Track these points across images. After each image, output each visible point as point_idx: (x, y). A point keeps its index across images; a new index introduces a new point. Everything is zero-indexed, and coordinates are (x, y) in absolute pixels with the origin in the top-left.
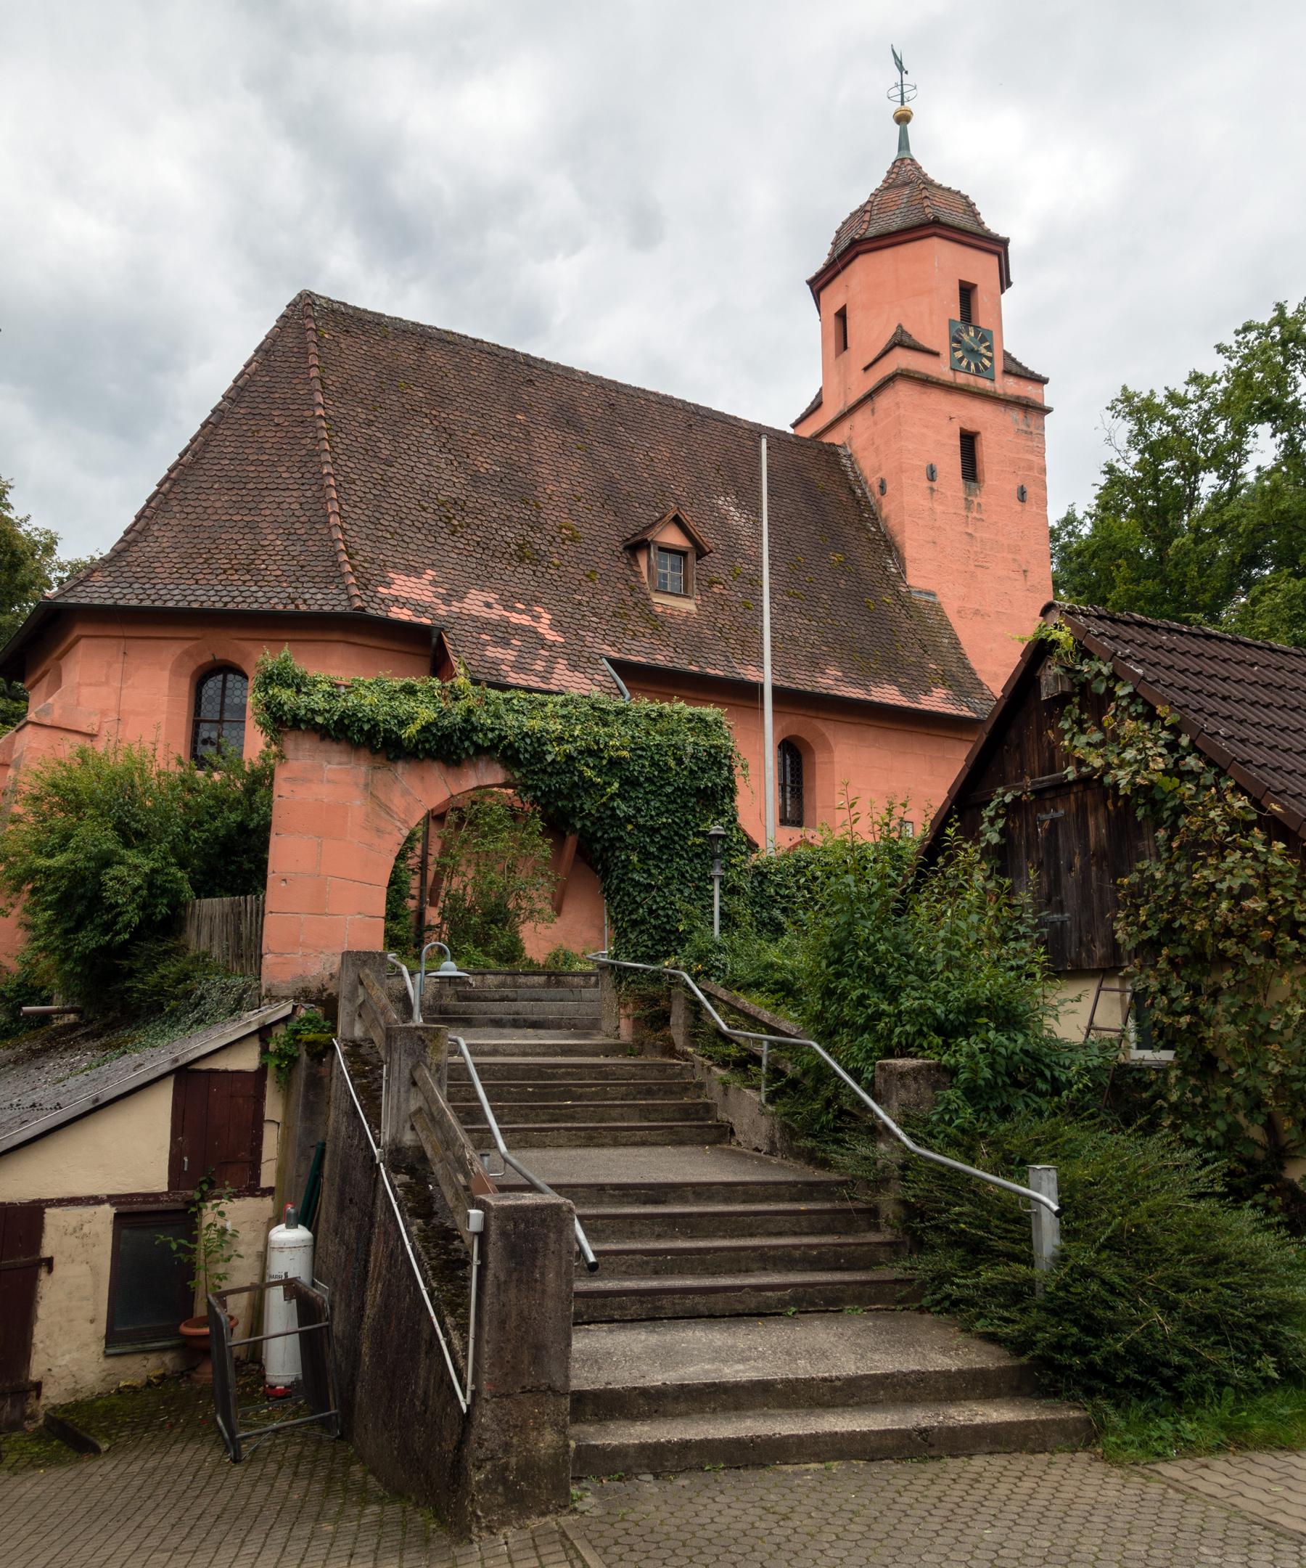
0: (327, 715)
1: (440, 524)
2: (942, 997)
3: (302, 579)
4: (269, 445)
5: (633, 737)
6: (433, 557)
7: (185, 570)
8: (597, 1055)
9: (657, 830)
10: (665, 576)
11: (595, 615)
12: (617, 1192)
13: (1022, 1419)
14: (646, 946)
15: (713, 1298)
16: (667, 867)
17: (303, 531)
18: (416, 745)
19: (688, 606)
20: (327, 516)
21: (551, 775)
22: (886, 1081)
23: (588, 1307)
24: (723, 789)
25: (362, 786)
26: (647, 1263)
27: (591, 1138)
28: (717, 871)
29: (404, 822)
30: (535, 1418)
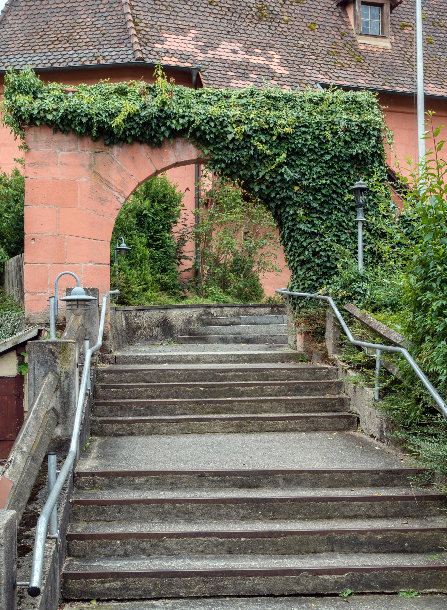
0: (54, 113)
3: (103, 43)
7: (28, 44)
8: (275, 361)
9: (319, 190)
10: (367, 23)
11: (313, 54)
12: (215, 478)
14: (312, 280)
15: (272, 579)
17: (104, 10)
18: (124, 132)
19: (385, 44)
21: (233, 150)
23: (156, 585)
24: (373, 155)
25: (87, 167)
26: (222, 544)
27: (241, 426)
28: (360, 217)
29: (121, 192)
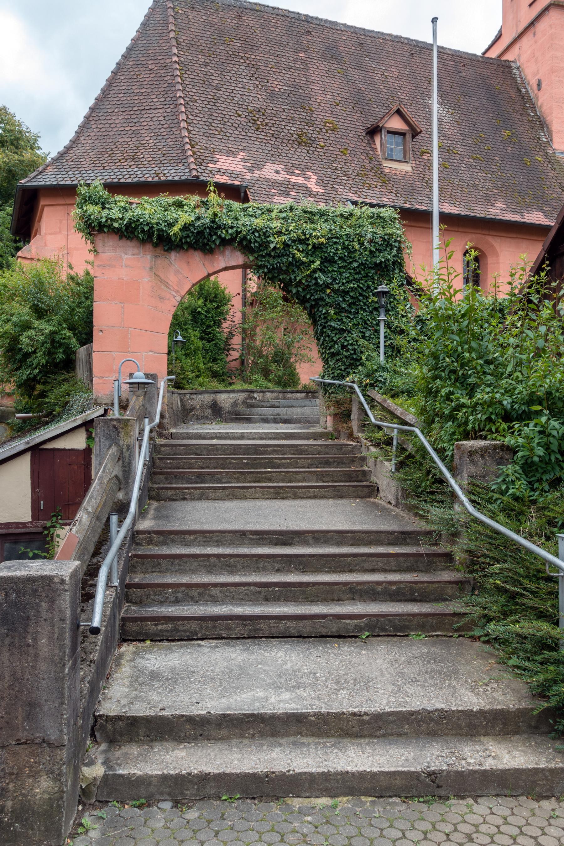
0: (120, 222)
1: (249, 124)
2: (509, 392)
4: (146, 83)
5: (331, 230)
6: (244, 145)
7: (98, 162)
8: (308, 439)
9: (348, 293)
12: (255, 537)
13: (531, 766)
14: (341, 370)
16: (355, 318)
17: (165, 133)
18: (181, 240)
19: (406, 168)
20: (179, 123)
22: (460, 458)
23: (202, 627)
26: (260, 592)
27: (278, 493)
28: (382, 316)
29: (177, 292)
30: (31, 767)
